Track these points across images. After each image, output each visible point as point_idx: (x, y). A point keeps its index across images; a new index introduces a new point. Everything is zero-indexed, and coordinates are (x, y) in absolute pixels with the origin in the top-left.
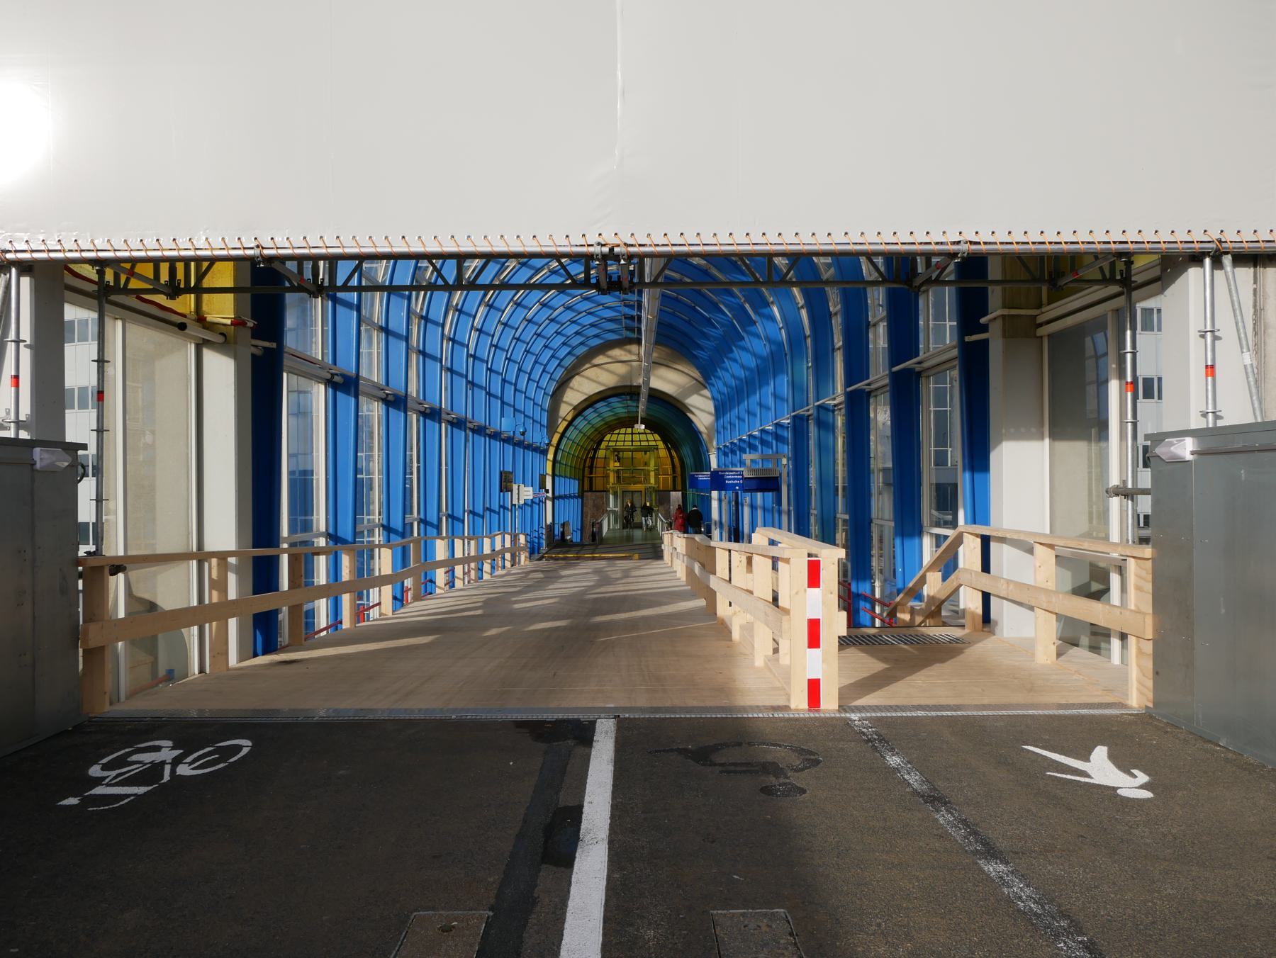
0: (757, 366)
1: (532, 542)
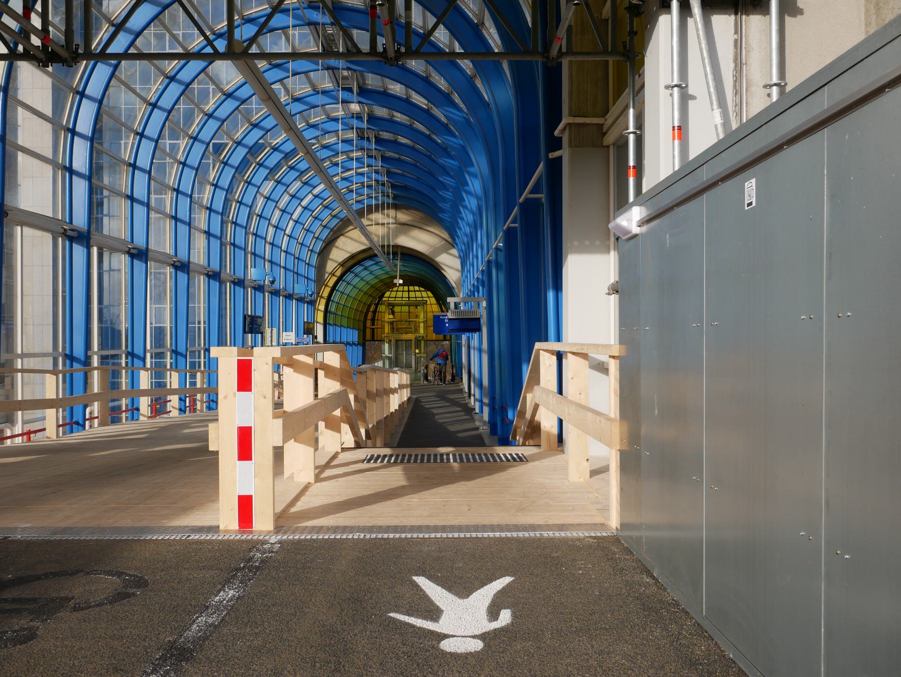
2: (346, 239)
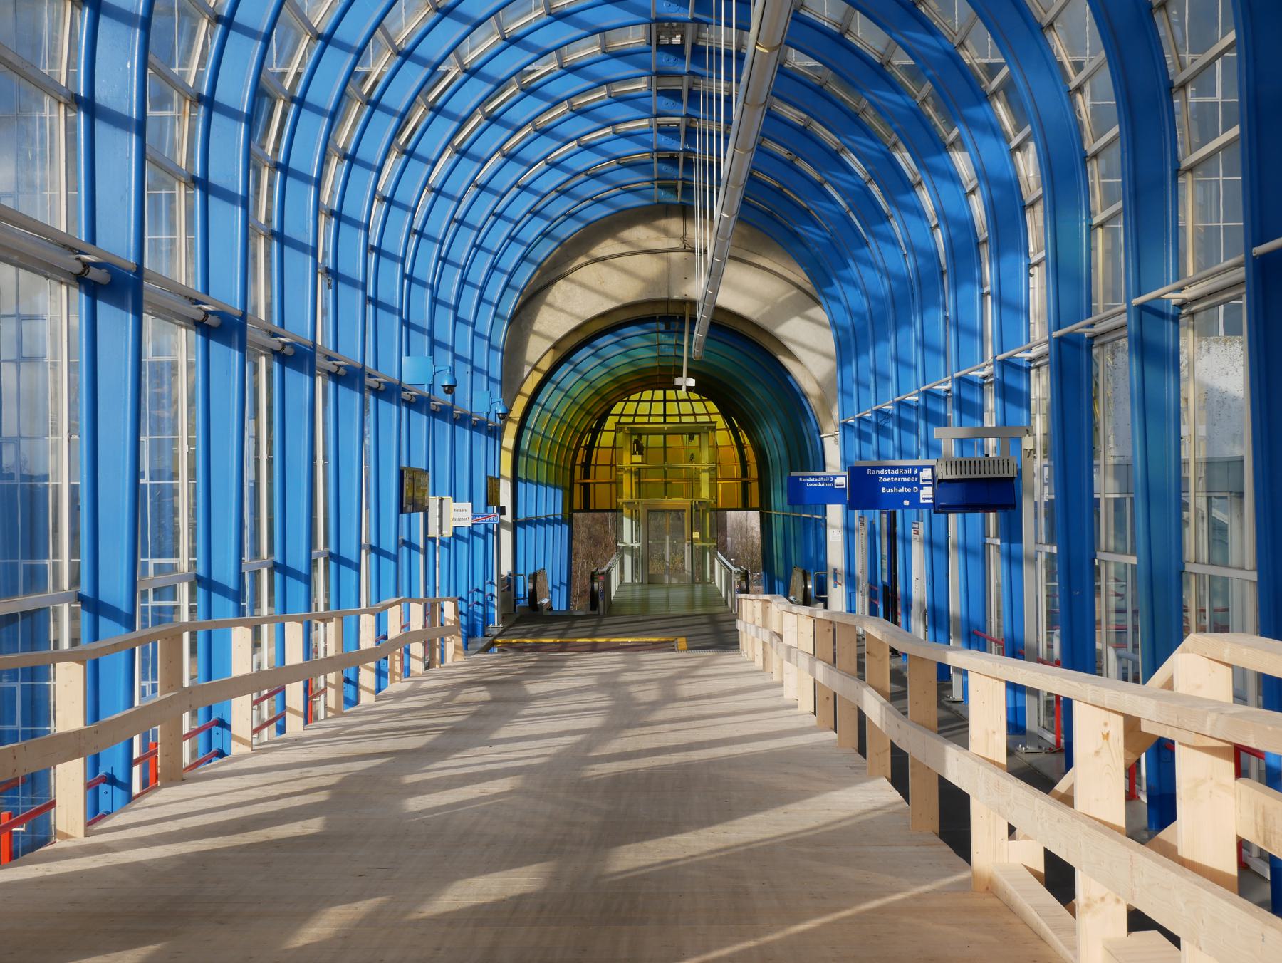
0: (891, 291)
1: (470, 614)
2: (573, 286)
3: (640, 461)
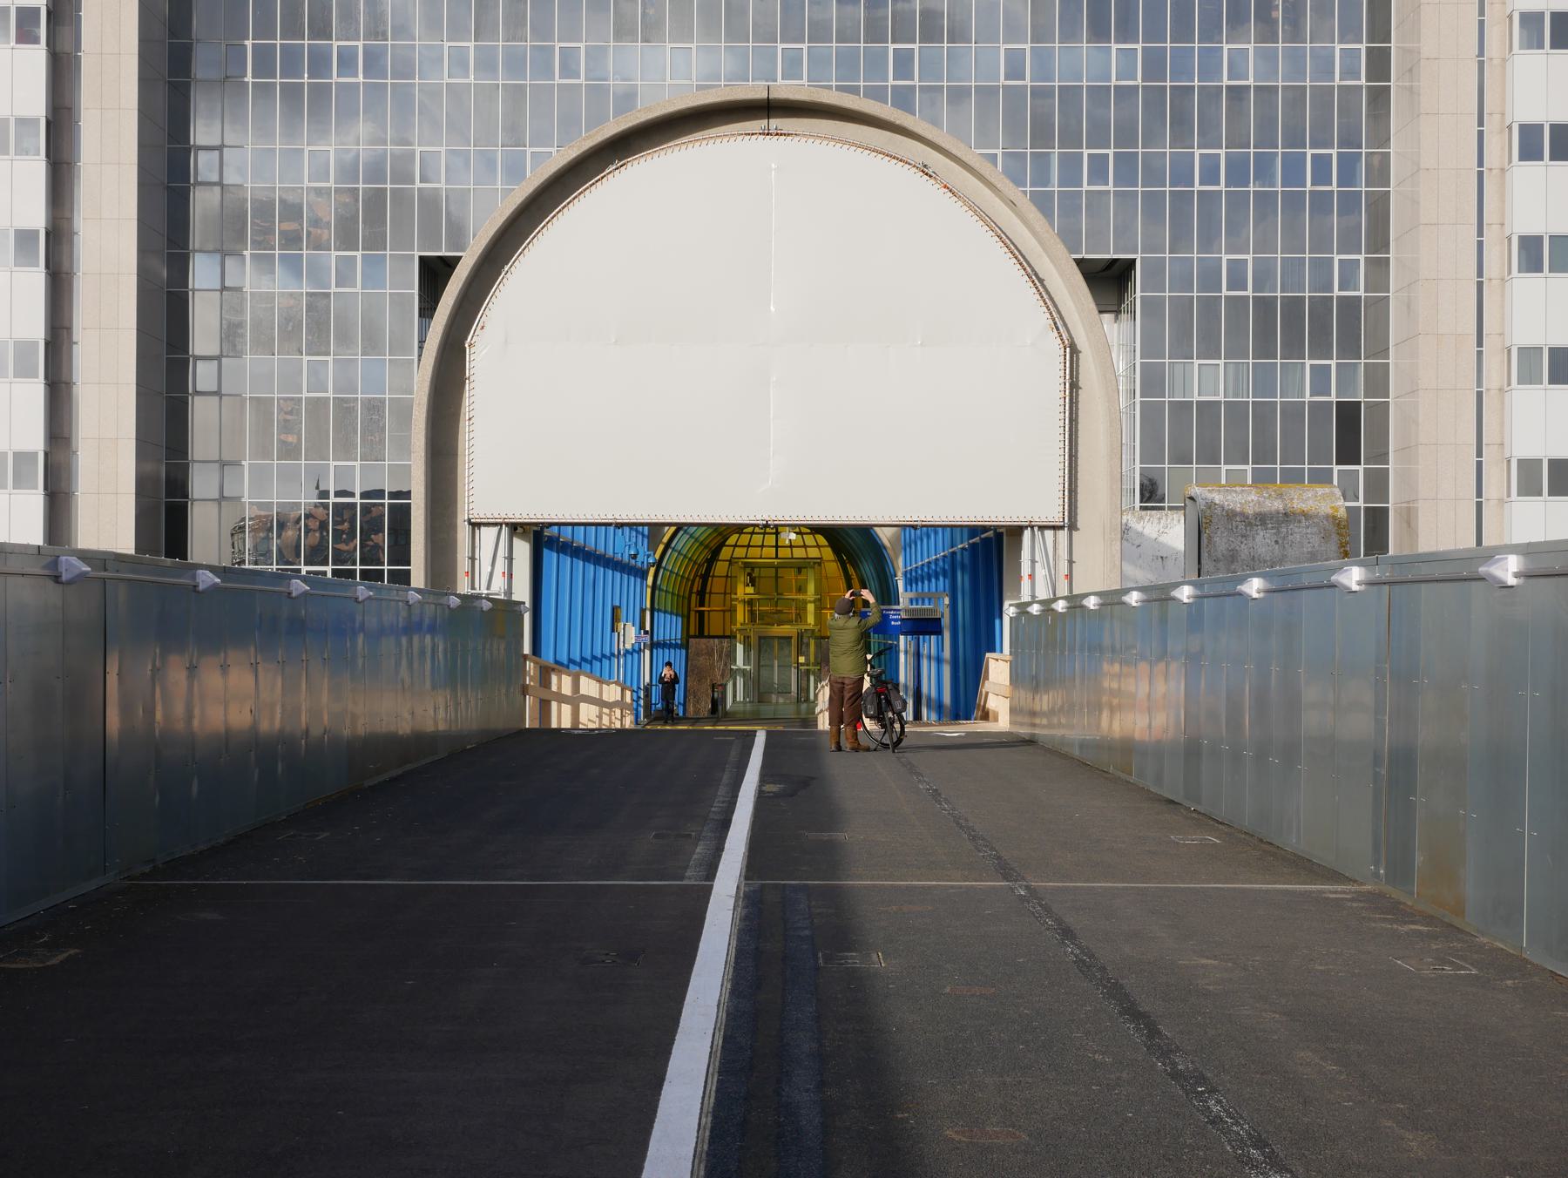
3: (752, 592)
